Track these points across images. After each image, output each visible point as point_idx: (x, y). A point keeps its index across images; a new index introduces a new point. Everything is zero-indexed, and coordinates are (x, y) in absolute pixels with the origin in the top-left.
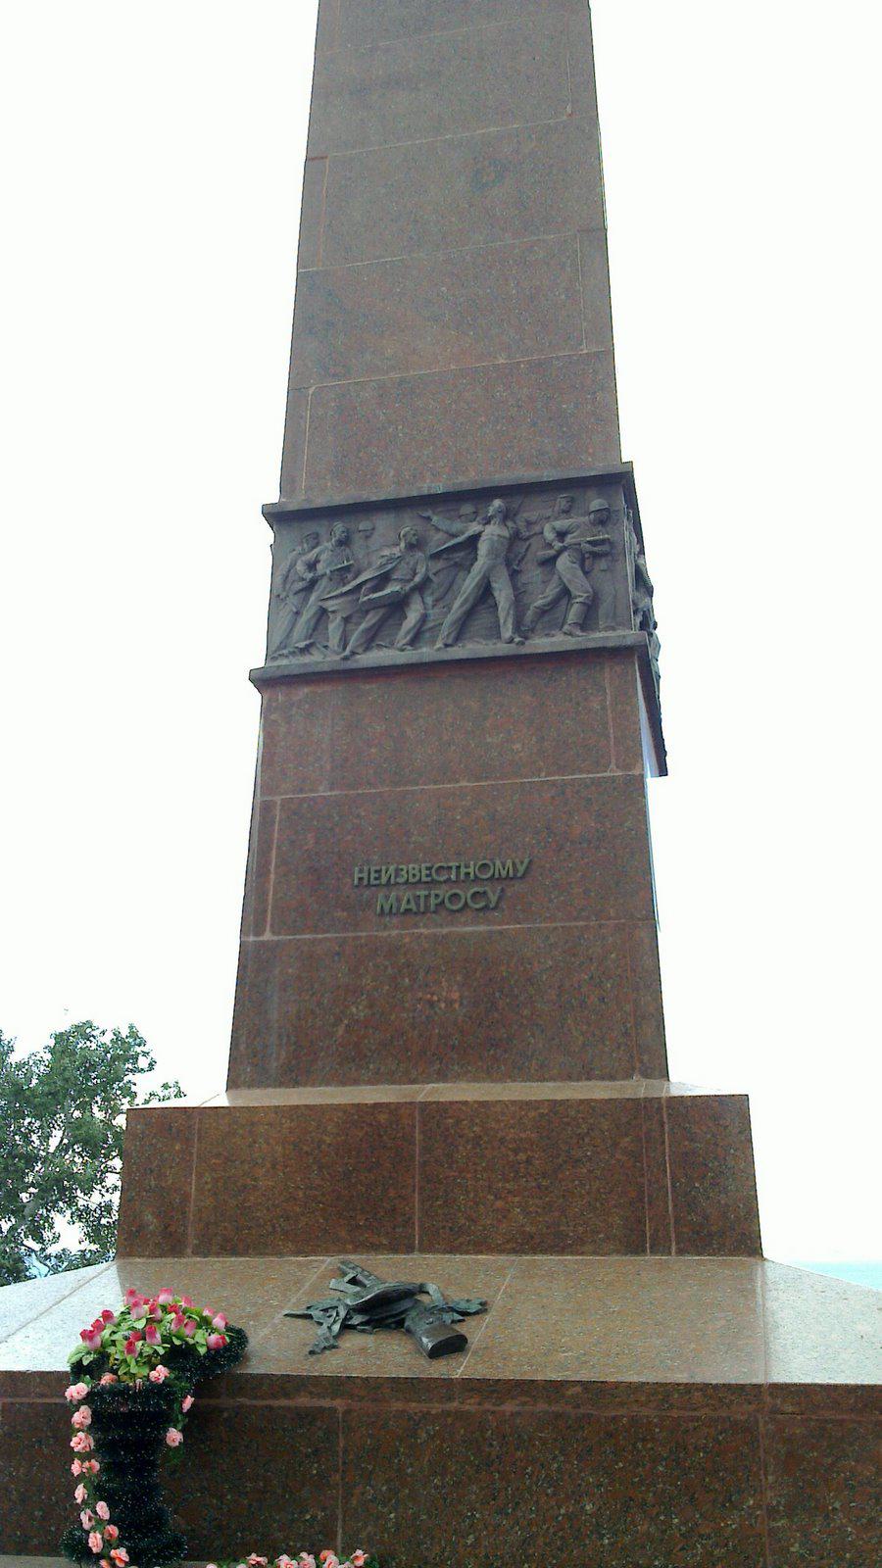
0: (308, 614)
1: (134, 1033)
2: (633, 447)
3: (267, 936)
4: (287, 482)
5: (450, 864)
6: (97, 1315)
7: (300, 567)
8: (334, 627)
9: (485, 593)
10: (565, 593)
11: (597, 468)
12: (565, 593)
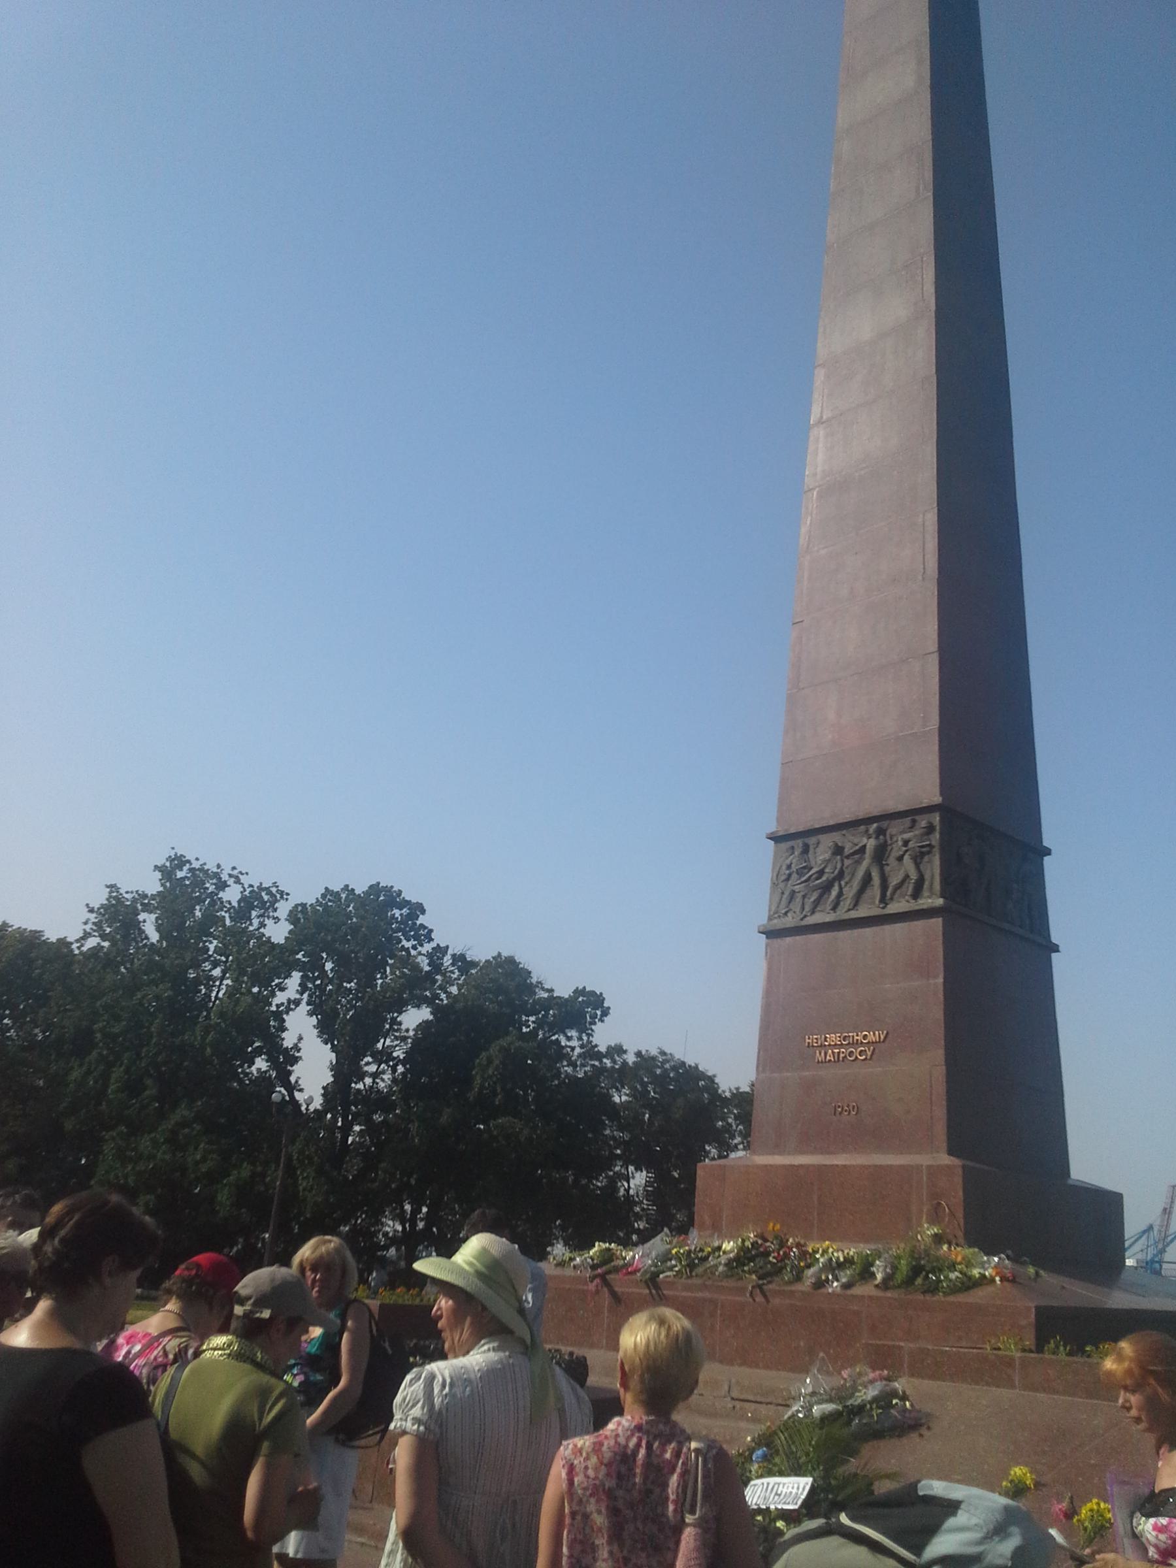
0: (787, 893)
5: (850, 1034)
7: (784, 867)
10: (907, 876)
12: (907, 876)
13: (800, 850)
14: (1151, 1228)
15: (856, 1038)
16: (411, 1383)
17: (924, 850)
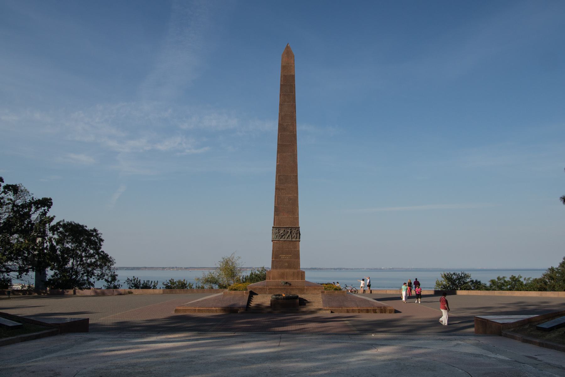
0: (276, 235)
1: (560, 263)
2: (300, 225)
3: (274, 259)
4: (274, 224)
6: (102, 237)
8: (278, 237)
9: (289, 235)
10: (295, 236)
11: (298, 227)
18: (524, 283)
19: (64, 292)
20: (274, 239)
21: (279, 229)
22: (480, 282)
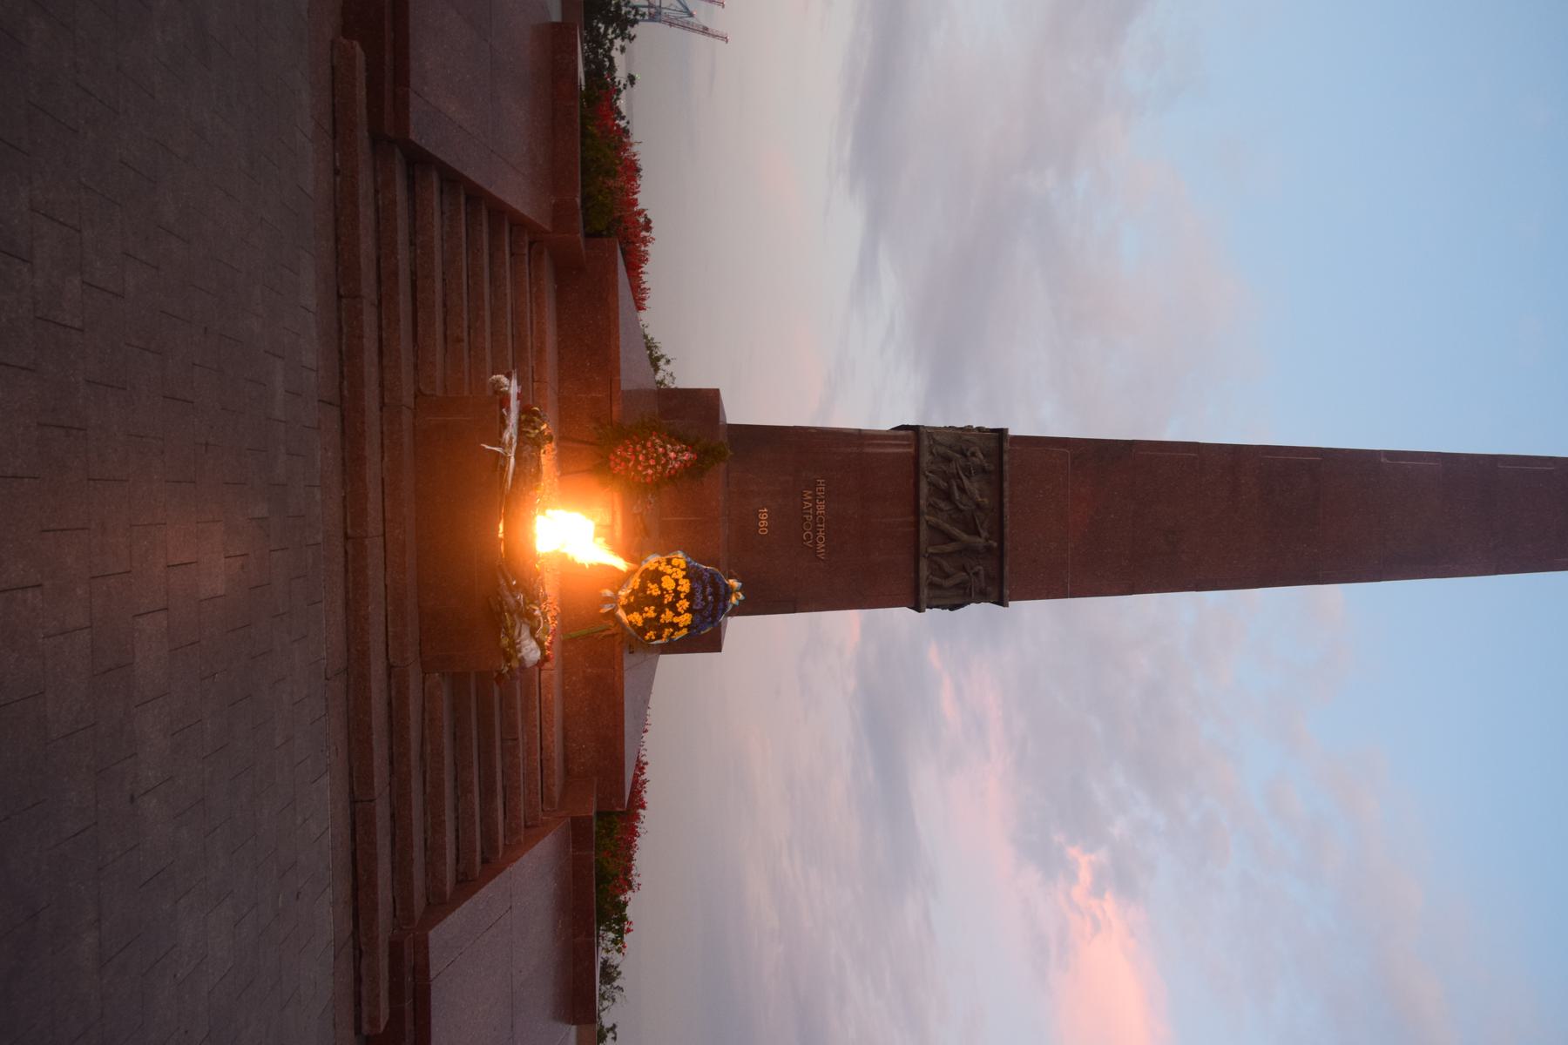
0: (950, 452)
9: (951, 538)
11: (1007, 592)
13: (986, 467)
14: (691, 15)
15: (821, 530)
16: (511, 438)
17: (968, 591)
18: (678, 605)
19: (669, 603)
20: (925, 442)
21: (996, 477)
22: (638, 170)
